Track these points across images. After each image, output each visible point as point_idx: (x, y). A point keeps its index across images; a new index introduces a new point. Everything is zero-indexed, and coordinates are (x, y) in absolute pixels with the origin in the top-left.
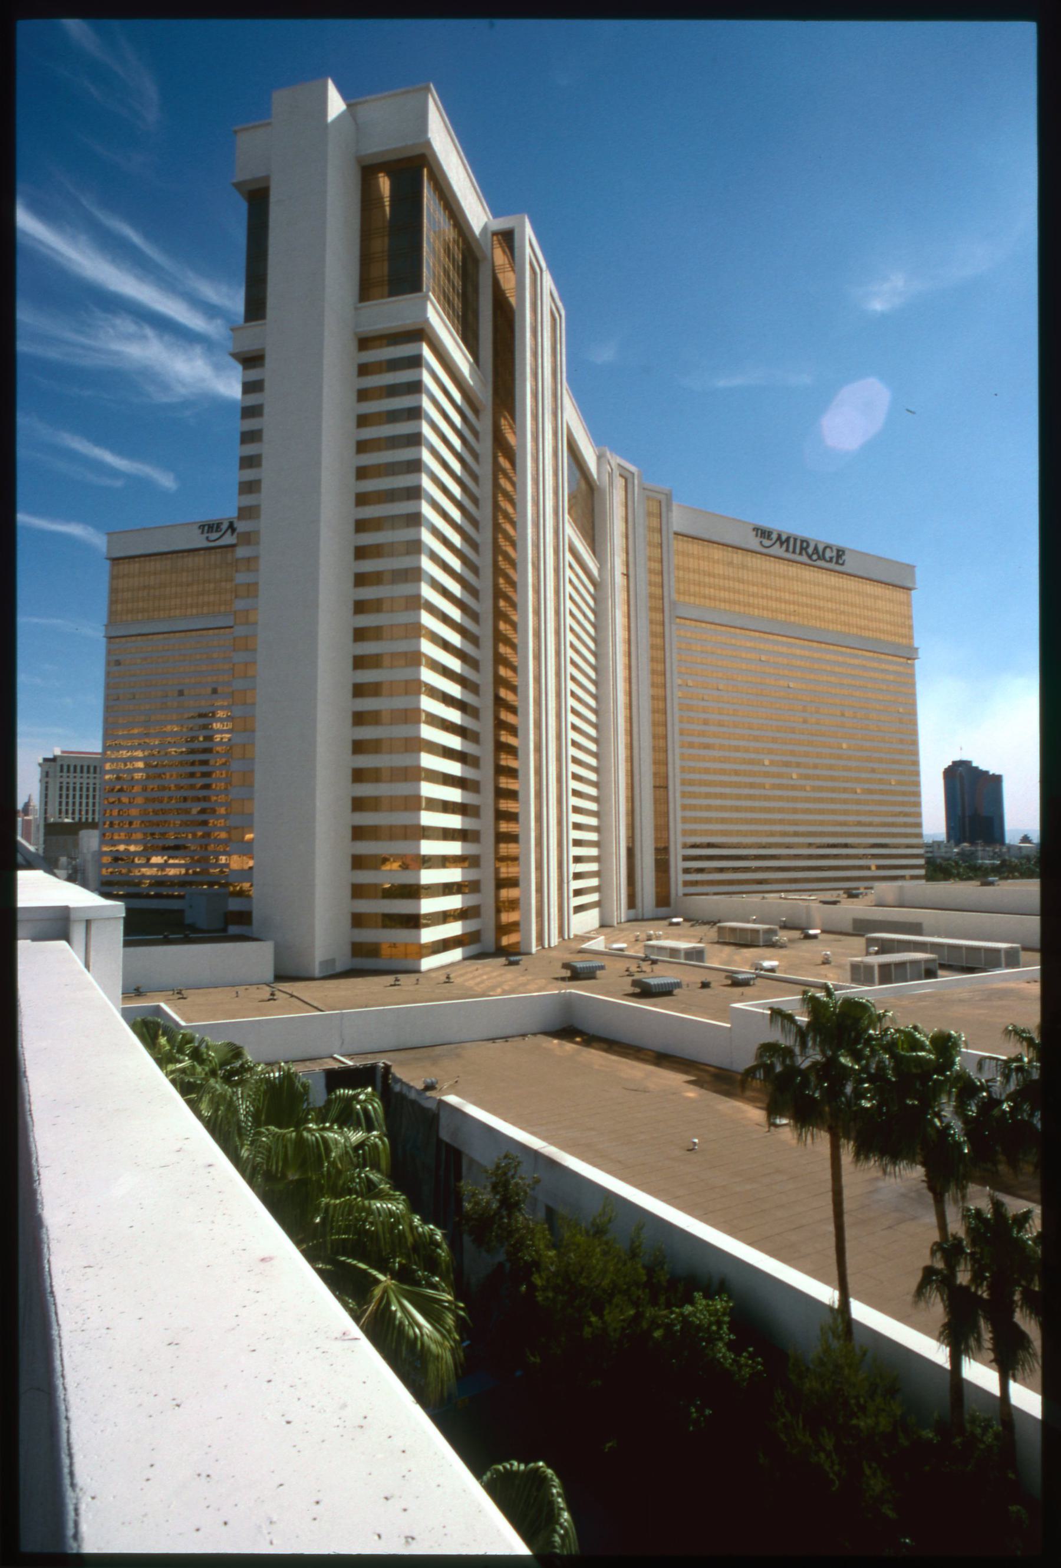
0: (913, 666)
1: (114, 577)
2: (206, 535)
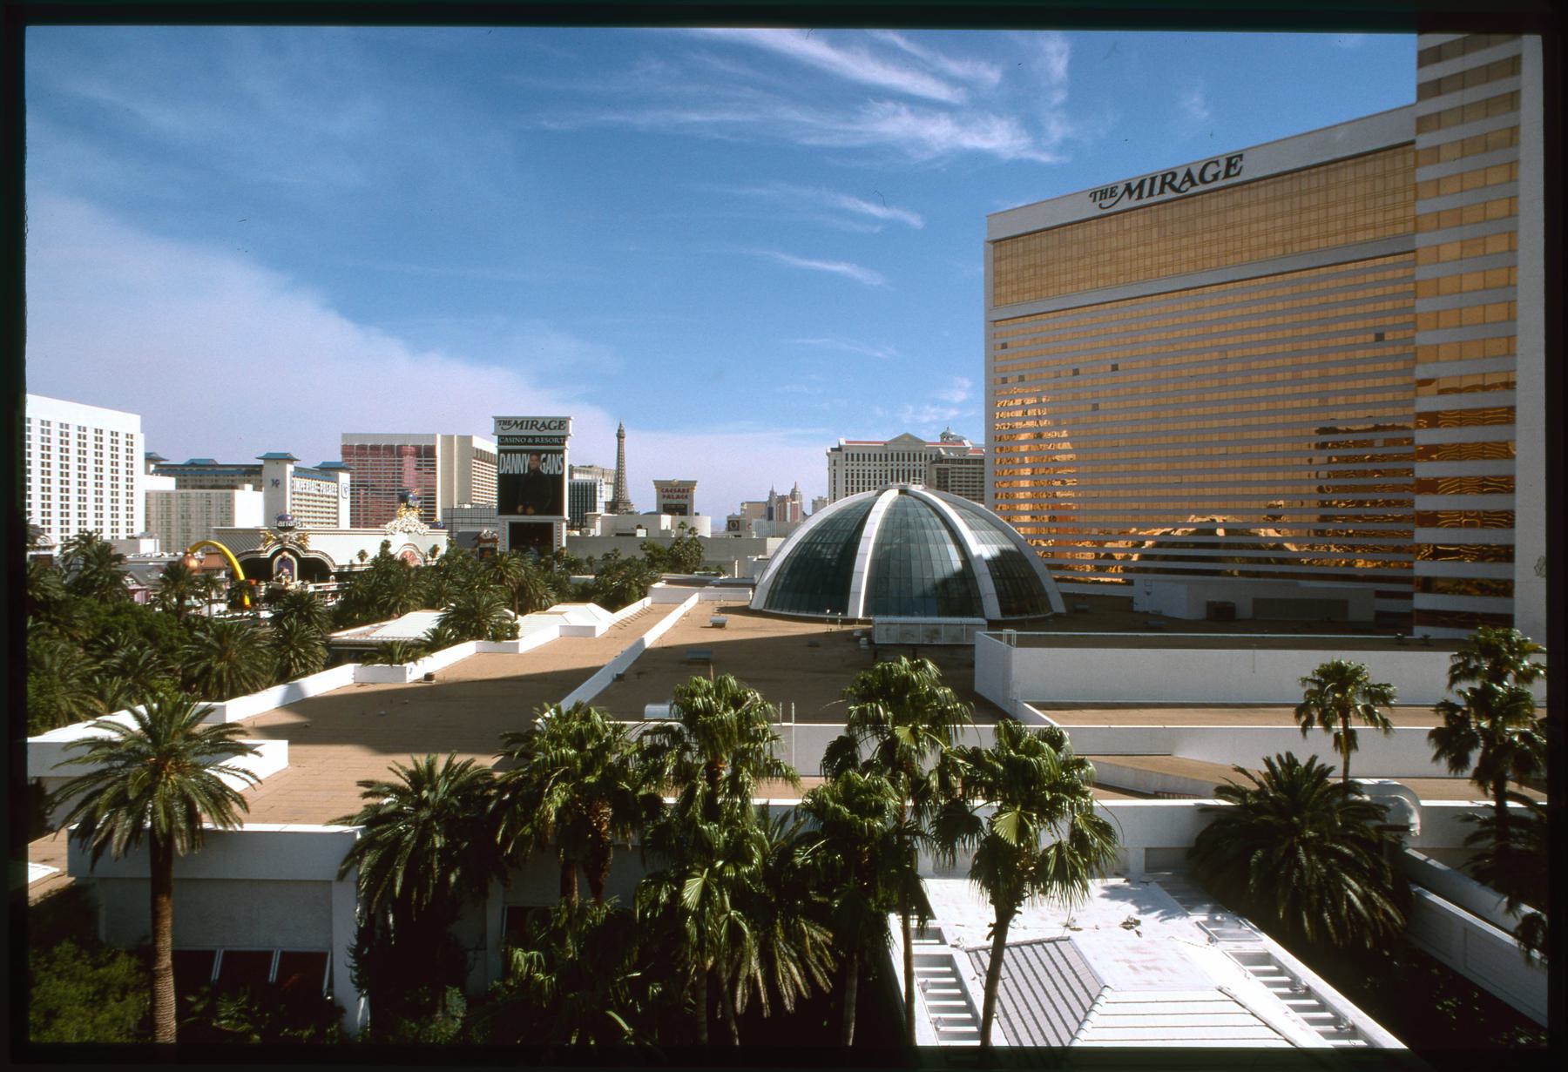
1: (997, 260)
2: (1098, 203)
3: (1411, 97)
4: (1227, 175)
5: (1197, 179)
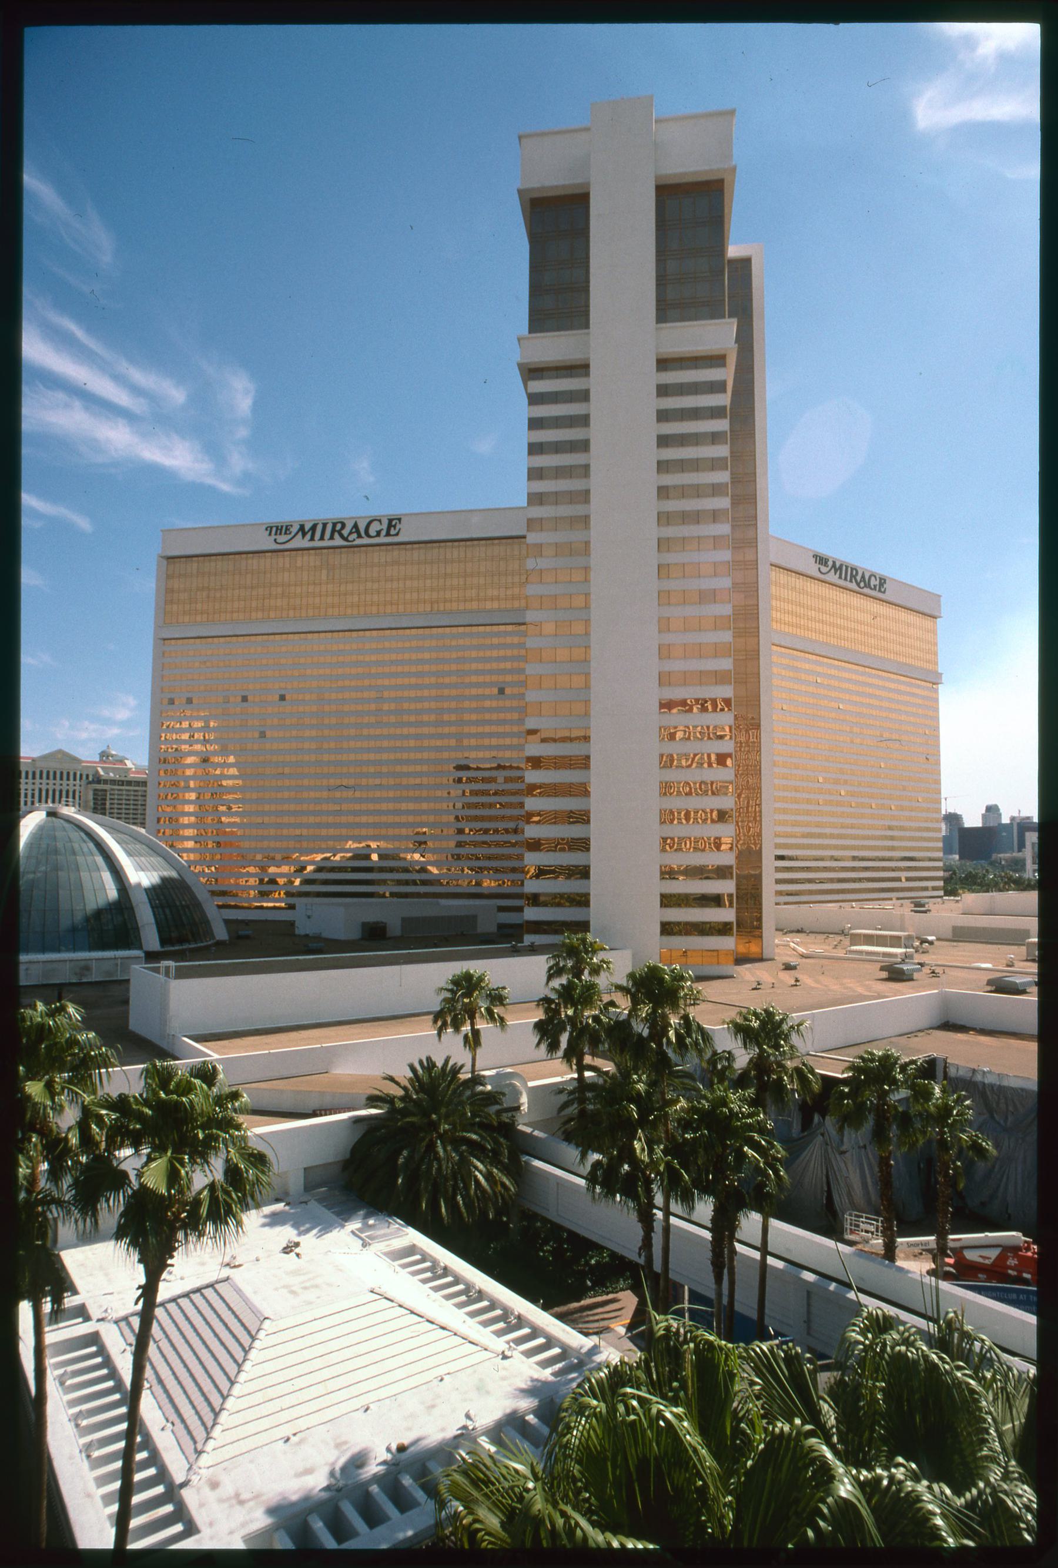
0: (936, 691)
2: (273, 537)
4: (388, 534)
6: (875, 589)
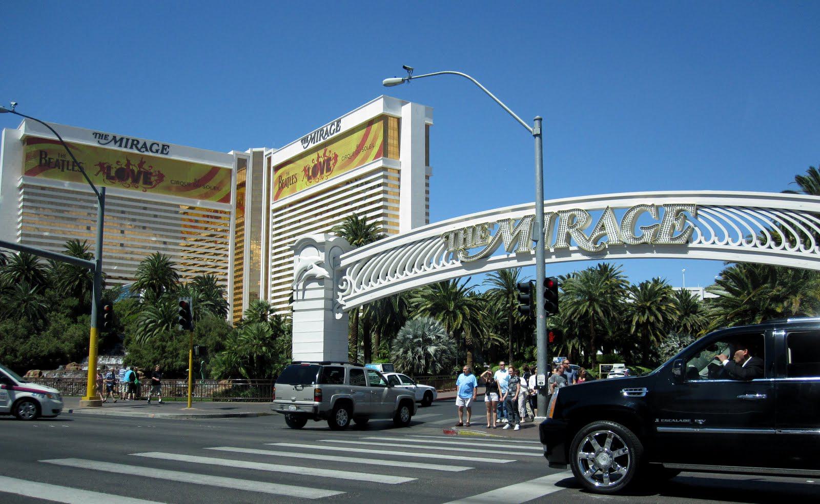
3: (342, 120)
5: (149, 149)
6: (157, 151)
